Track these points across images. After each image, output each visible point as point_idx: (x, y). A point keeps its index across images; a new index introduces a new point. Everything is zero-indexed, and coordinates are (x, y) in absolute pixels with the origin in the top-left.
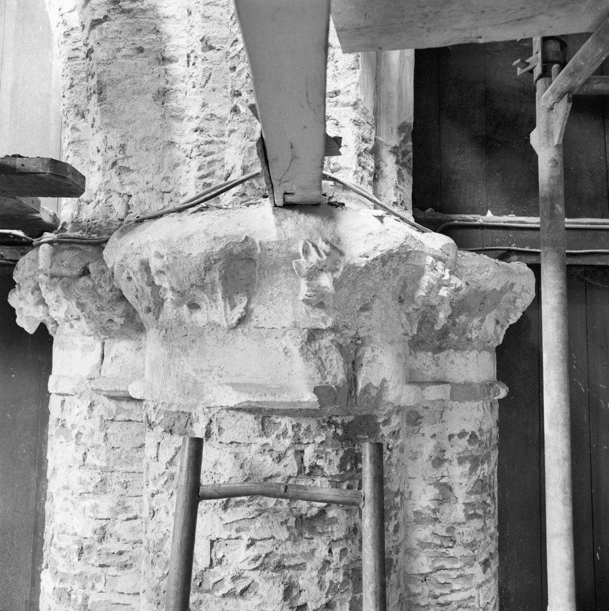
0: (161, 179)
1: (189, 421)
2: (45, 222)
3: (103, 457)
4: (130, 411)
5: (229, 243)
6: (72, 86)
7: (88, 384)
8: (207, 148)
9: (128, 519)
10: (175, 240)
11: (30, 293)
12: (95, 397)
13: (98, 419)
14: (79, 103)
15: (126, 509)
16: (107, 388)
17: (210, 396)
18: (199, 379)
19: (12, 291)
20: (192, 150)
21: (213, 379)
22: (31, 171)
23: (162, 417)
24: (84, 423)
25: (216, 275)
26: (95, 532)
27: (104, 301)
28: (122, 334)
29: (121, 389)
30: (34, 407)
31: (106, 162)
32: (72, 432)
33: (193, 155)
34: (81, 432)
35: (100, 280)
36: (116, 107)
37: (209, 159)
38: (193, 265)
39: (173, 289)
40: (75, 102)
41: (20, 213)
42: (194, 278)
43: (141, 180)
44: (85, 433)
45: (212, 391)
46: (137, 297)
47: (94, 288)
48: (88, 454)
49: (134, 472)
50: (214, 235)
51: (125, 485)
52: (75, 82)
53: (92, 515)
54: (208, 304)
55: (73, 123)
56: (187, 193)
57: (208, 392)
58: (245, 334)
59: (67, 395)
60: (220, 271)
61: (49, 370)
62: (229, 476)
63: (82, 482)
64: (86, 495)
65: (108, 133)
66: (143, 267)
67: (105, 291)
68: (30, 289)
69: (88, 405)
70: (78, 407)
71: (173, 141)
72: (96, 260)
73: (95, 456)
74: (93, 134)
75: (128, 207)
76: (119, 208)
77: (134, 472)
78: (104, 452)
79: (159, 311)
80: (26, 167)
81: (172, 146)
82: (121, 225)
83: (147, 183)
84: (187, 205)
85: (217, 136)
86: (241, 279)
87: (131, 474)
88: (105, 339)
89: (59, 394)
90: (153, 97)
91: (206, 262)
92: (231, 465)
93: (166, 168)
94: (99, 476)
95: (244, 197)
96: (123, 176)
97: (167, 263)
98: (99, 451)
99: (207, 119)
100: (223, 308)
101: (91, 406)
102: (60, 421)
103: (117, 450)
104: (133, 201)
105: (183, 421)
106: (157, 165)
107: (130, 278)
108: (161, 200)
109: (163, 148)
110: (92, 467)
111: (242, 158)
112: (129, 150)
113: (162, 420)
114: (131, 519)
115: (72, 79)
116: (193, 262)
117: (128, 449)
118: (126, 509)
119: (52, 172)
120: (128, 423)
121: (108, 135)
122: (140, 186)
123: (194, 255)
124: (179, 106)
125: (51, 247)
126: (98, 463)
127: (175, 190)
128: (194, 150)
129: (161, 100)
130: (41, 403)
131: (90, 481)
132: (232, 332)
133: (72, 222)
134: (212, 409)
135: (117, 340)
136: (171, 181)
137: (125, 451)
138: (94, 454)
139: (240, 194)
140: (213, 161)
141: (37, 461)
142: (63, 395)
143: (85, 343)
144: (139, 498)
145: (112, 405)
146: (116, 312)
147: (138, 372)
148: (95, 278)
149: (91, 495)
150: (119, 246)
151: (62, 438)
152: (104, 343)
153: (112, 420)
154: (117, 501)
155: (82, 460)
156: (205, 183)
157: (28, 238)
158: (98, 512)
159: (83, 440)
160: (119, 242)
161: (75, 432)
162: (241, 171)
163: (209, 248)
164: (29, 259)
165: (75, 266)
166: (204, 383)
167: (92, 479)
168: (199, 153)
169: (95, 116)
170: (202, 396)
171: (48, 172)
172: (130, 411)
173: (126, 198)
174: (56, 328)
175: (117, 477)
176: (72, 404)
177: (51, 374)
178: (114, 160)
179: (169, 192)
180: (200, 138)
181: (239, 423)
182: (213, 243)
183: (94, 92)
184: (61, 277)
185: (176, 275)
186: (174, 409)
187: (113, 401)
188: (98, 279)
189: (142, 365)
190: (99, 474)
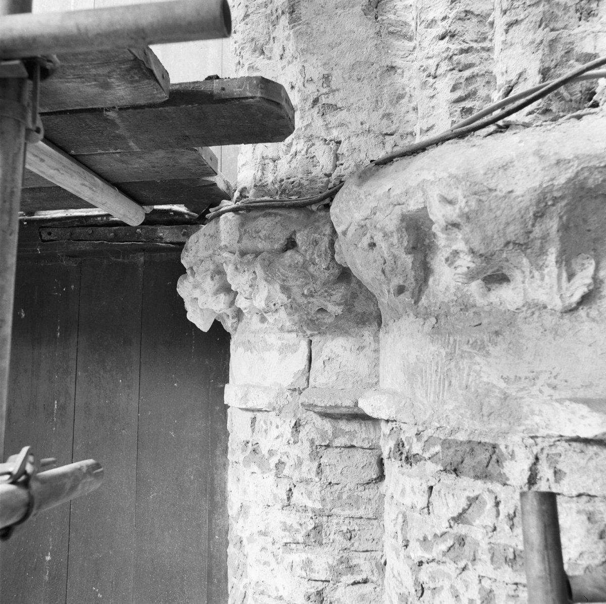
0: (380, 117)
1: (494, 457)
2: (218, 188)
3: (316, 495)
4: (352, 434)
5: (582, 169)
6: (247, 16)
7: (289, 397)
8: (464, 59)
9: (355, 583)
10: (482, 172)
11: (209, 278)
12: (303, 415)
13: (307, 444)
14: (257, 35)
15: (351, 569)
16: (323, 402)
17: (537, 419)
18: (512, 391)
19: (181, 278)
20: (438, 65)
21: (541, 391)
22: (236, 95)
23: (438, 448)
24: (286, 448)
25: (552, 225)
26: (309, 598)
27: (318, 282)
28: (338, 328)
29: (344, 405)
30: (202, 423)
31: (305, 100)
32: (270, 461)
33: (441, 71)
34: (283, 460)
35: (313, 254)
36: (315, 27)
37: (467, 73)
38: (515, 210)
39: (472, 251)
40: (252, 36)
41: (193, 177)
42: (514, 231)
43: (353, 120)
44: (290, 462)
45: (540, 411)
46: (383, 272)
47: (305, 266)
48: (295, 491)
49: (361, 518)
50: (557, 157)
51: (349, 535)
52: (250, 11)
53: (304, 574)
54: (527, 273)
55: (250, 62)
56: (433, 126)
57: (533, 413)
58: (593, 320)
59: (260, 410)
60: (561, 218)
61: (224, 377)
62: (580, 549)
63: (286, 528)
64: (293, 546)
65: (305, 61)
66: (404, 224)
67: (321, 268)
68: (209, 273)
69: (293, 424)
70: (277, 427)
71: (394, 65)
72: (305, 227)
73: (304, 495)
74: (283, 68)
75: (337, 157)
76: (324, 160)
77: (361, 518)
78: (316, 489)
79: (420, 291)
80: (227, 91)
81: (392, 73)
82: (329, 181)
83: (362, 124)
84: (464, 128)
85: (476, 41)
86: (589, 231)
87: (356, 521)
88: (312, 335)
89: (247, 410)
90: (363, 10)
91: (539, 202)
92: (583, 532)
93: (386, 102)
94: (311, 521)
95: (548, 114)
96: (328, 116)
97: (467, 210)
98: (309, 487)
99: (460, 19)
100: (555, 281)
101: (297, 426)
102: (250, 444)
103: (336, 486)
104: (343, 148)
105: (483, 456)
106: (374, 100)
107: (372, 245)
108: (382, 145)
109: (381, 75)
110: (300, 509)
111: (540, 56)
112: (335, 82)
113: (437, 453)
114: (359, 583)
115: (247, 6)
116: (514, 204)
117: (352, 486)
118: (351, 569)
119: (263, 96)
120: (350, 449)
121: (305, 65)
122: (352, 128)
123: (519, 191)
124: (399, 19)
125: (237, 216)
126: (310, 504)
127: (401, 131)
128: (442, 64)
129: (373, 13)
130: (210, 418)
131: (299, 527)
132: (567, 316)
133: (255, 186)
134: (539, 440)
135: (329, 336)
136: (395, 119)
137: (347, 489)
138: (303, 491)
139: (540, 111)
140: (473, 76)
141: (208, 490)
142: (253, 411)
143: (285, 342)
144: (368, 553)
145: (327, 425)
146: (333, 298)
147: (362, 380)
148: (306, 251)
149: (301, 547)
150: (363, 197)
151: (254, 468)
152: (311, 341)
153: (328, 446)
154: (338, 558)
155: (286, 497)
156: (463, 108)
157: (192, 213)
158: (312, 570)
159: (286, 471)
160: (362, 192)
161: (274, 460)
162: (539, 78)
163: (547, 178)
164: (205, 235)
165: (277, 236)
166: (522, 398)
167: (301, 525)
168: (452, 67)
169: (286, 42)
170: (519, 419)
171: (259, 95)
172: (352, 434)
173: (333, 145)
174: (238, 324)
175: (337, 524)
176: (268, 423)
177: (226, 381)
178: (315, 97)
179: (392, 134)
180: (451, 46)
181: (592, 464)
182: (555, 170)
183: (283, 13)
184: (257, 254)
185: (482, 227)
186: (461, 437)
187: (328, 420)
188: (309, 252)
189: (398, 373)
190: (312, 518)
